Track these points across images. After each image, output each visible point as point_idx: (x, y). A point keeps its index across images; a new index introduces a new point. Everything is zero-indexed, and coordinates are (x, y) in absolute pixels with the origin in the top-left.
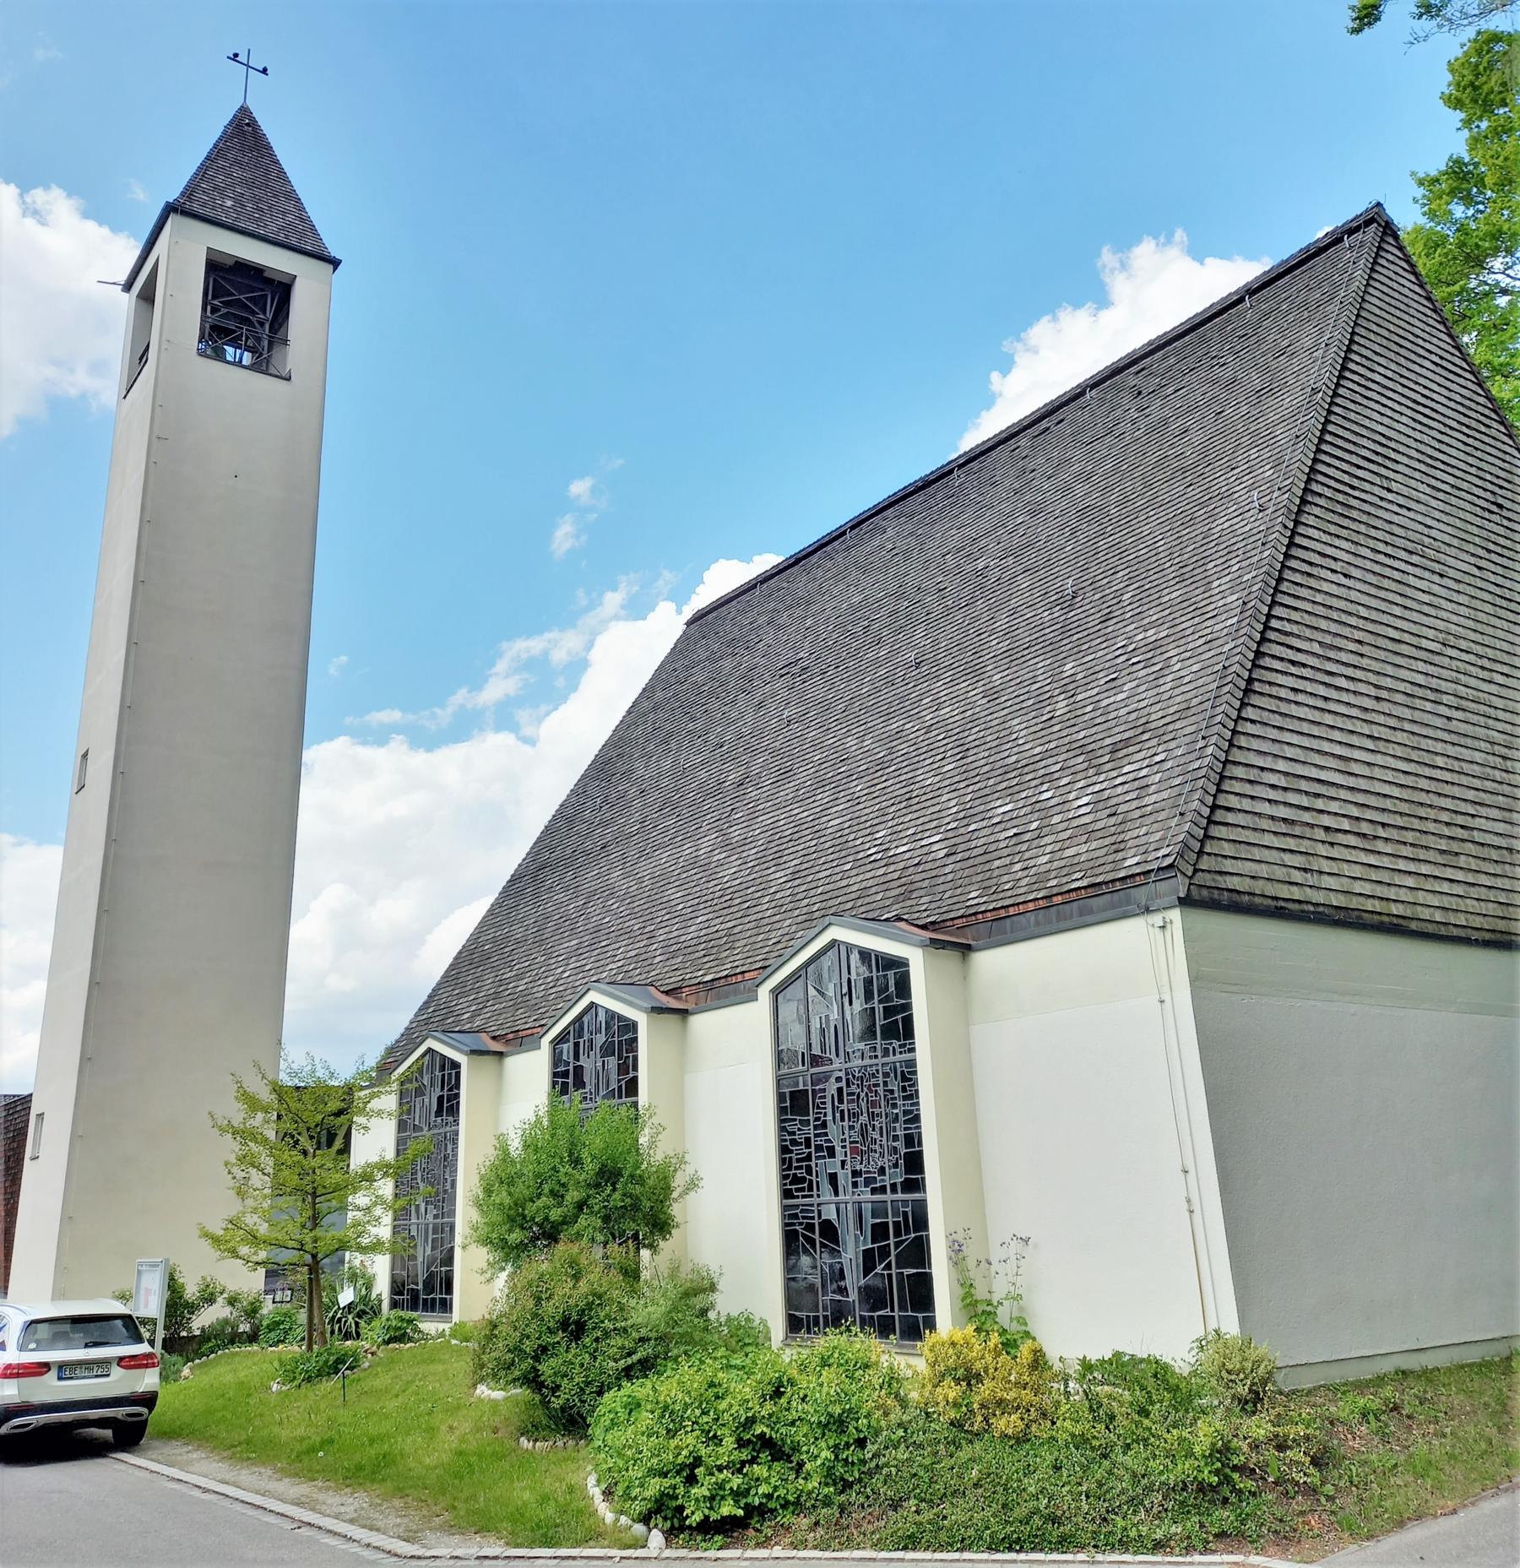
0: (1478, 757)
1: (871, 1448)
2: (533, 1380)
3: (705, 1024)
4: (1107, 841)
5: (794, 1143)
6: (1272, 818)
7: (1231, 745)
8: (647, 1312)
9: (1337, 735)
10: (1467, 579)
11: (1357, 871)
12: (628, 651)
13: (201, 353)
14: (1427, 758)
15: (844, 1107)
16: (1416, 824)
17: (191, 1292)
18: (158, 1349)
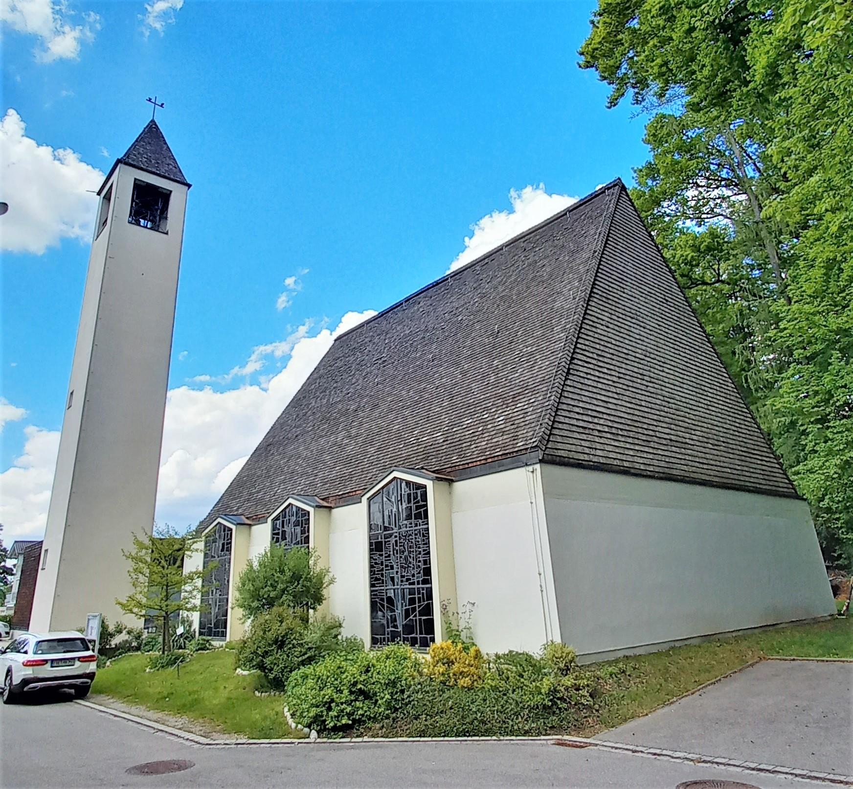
0: (658, 402)
1: (407, 693)
2: (261, 667)
3: (339, 513)
5: (376, 563)
6: (577, 426)
7: (561, 396)
8: (312, 636)
9: (603, 392)
12: (309, 352)
16: (634, 429)
17: (111, 628)
18: (96, 653)
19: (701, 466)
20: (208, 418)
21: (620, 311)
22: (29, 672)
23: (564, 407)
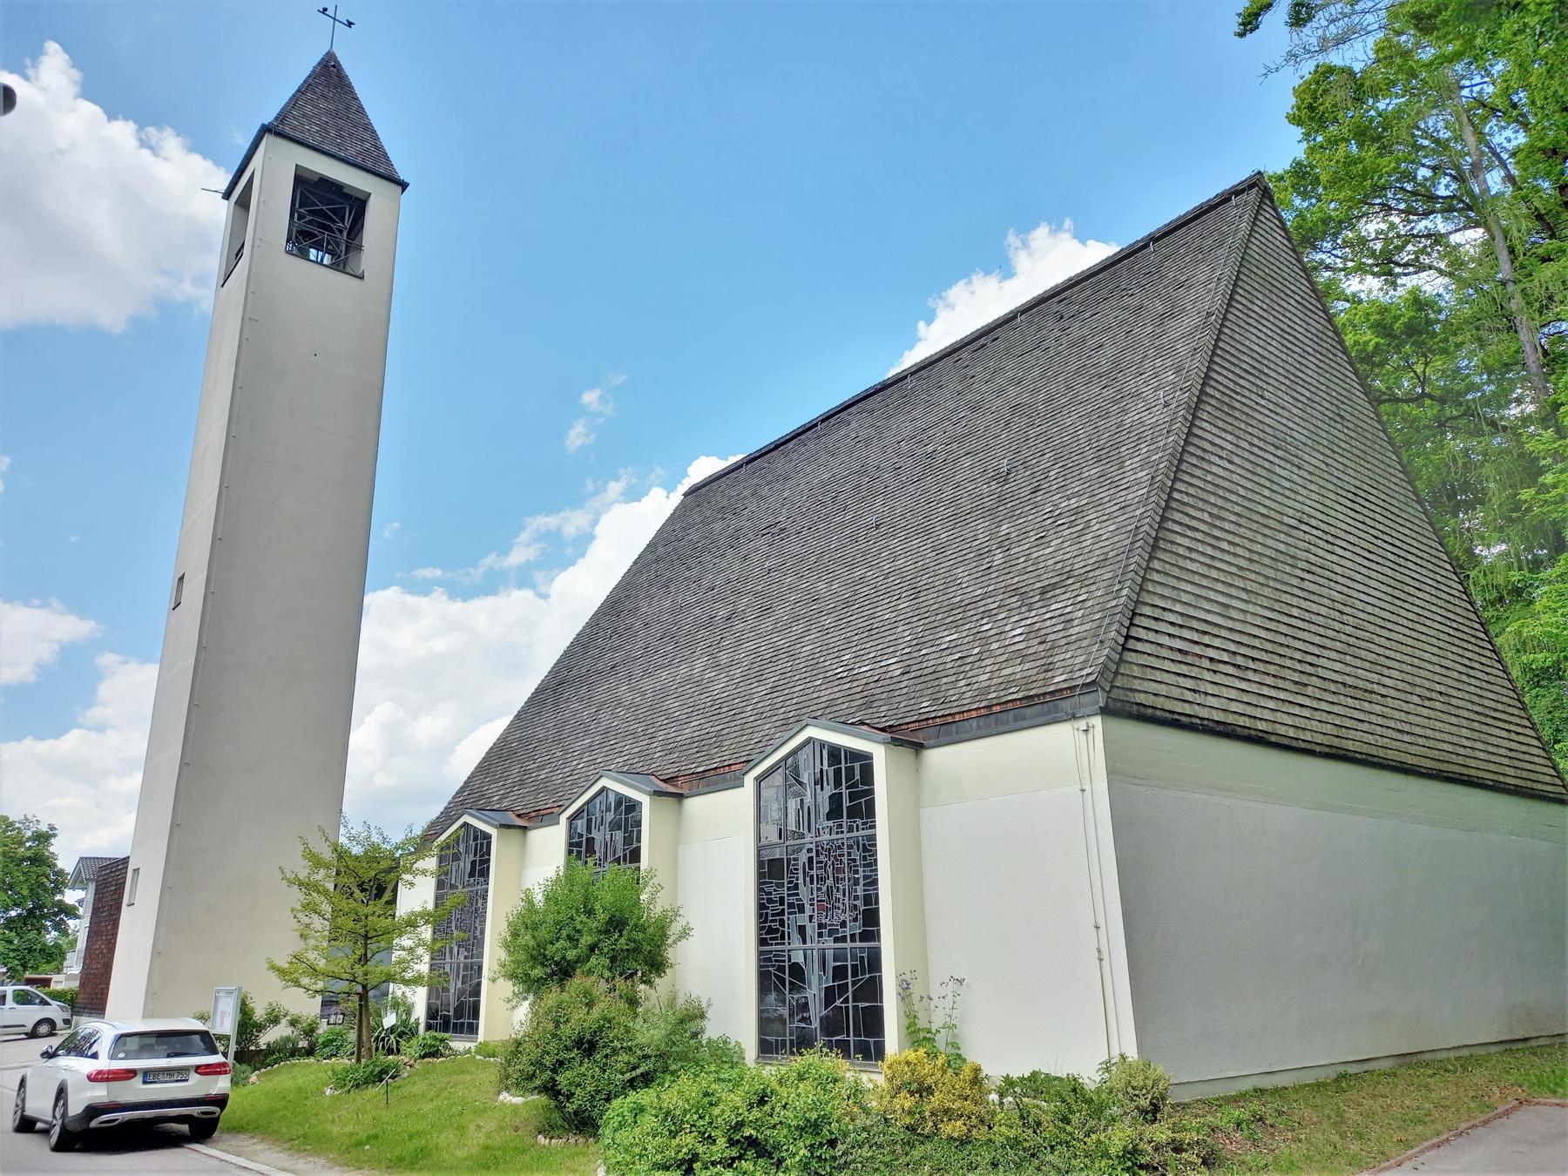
0: (1323, 610)
1: (841, 1147)
2: (551, 1089)
3: (698, 806)
4: (1038, 663)
5: (770, 901)
6: (1171, 648)
7: (1141, 589)
8: (649, 1034)
9: (1220, 587)
10: (1317, 472)
11: (1233, 694)
12: (629, 525)
13: (289, 252)
14: (1286, 609)
15: (814, 872)
16: (1277, 660)
17: (259, 1014)
18: (231, 1060)
19: (1399, 736)
20: (439, 645)
21: (1255, 432)
22: (100, 1093)
23: (1147, 611)
